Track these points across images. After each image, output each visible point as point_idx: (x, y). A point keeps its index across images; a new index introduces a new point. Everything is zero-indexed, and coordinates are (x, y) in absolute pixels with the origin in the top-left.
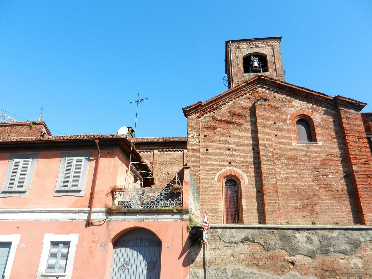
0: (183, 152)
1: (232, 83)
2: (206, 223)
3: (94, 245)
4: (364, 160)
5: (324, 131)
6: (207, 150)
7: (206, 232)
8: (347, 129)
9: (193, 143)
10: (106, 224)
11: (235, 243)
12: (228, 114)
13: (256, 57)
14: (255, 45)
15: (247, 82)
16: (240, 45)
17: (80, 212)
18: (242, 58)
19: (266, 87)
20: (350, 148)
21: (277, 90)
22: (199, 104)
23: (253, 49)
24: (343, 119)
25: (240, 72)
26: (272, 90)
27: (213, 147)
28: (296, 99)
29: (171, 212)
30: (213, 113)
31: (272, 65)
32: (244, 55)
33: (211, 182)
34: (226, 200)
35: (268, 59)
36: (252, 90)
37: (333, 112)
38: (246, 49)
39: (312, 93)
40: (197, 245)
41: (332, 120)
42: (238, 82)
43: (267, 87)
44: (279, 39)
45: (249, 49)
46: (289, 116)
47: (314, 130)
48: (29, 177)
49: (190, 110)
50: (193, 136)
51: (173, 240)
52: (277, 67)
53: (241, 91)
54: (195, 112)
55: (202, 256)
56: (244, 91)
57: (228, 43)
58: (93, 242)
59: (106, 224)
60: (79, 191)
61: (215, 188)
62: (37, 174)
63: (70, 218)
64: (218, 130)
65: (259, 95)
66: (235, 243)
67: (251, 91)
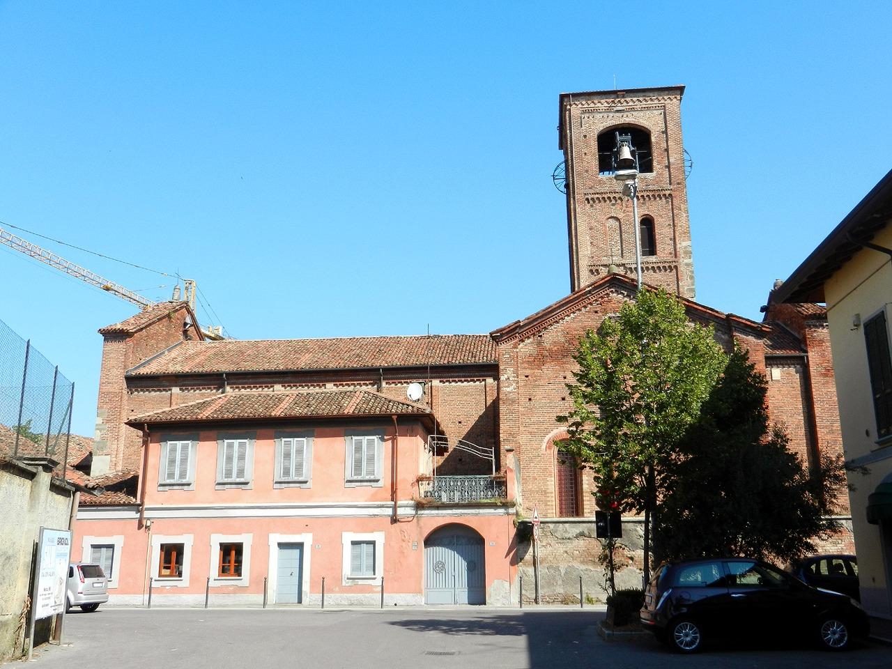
0: (483, 383)
1: (574, 198)
2: (536, 518)
3: (404, 544)
6: (530, 399)
7: (536, 527)
9: (508, 389)
11: (569, 539)
13: (626, 135)
14: (625, 104)
16: (592, 105)
17: (382, 506)
18: (596, 137)
19: (624, 292)
22: (516, 325)
25: (590, 172)
27: (539, 394)
29: (494, 506)
30: (539, 336)
31: (661, 154)
32: (601, 129)
34: (560, 476)
35: (653, 139)
36: (602, 297)
37: (725, 337)
38: (606, 115)
39: (695, 306)
40: (526, 542)
42: (587, 196)
43: (626, 293)
45: (611, 115)
48: (307, 462)
49: (502, 335)
51: (497, 537)
52: (672, 160)
54: (510, 338)
56: (589, 299)
57: (566, 100)
58: (404, 541)
60: (377, 481)
64: (547, 365)
65: (614, 305)
66: (569, 539)
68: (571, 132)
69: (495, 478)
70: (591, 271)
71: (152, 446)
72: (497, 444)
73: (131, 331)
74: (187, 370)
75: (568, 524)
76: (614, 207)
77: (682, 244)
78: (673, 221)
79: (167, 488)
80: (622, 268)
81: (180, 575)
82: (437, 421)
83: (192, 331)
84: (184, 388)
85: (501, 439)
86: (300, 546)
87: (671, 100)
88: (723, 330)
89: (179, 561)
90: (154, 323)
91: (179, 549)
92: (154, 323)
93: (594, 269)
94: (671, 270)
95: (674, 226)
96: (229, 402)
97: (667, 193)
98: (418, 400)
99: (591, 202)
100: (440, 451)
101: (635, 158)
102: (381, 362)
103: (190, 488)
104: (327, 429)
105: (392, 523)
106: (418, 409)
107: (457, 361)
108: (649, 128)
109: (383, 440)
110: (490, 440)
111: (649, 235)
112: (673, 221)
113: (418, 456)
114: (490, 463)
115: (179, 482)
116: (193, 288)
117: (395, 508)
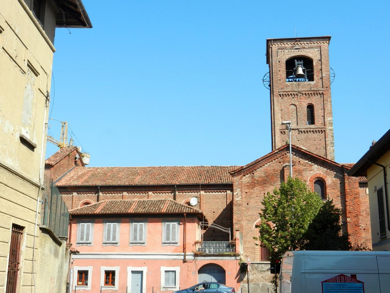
2: (249, 261)
3: (189, 273)
4: (355, 214)
5: (332, 191)
6: (248, 204)
8: (348, 190)
9: (238, 199)
10: (194, 261)
12: (264, 175)
13: (301, 61)
14: (300, 45)
15: (279, 149)
16: (283, 45)
17: (179, 255)
18: (285, 62)
19: (293, 153)
20: (347, 205)
21: (302, 156)
22: (242, 168)
23: (298, 50)
24: (346, 183)
26: (298, 156)
27: (252, 202)
28: (315, 164)
31: (318, 72)
32: (288, 58)
33: (250, 228)
35: (314, 64)
36: (283, 155)
37: (341, 176)
38: (290, 51)
39: (327, 161)
41: (339, 182)
42: (279, 93)
43: (294, 153)
44: (328, 39)
45: (293, 50)
46: (309, 178)
47: (326, 190)
49: (235, 173)
50: (238, 194)
51: (232, 270)
52: (324, 75)
53: (274, 156)
55: (247, 278)
56: (277, 156)
57: (270, 42)
58: (189, 271)
59: (194, 261)
60: (177, 243)
61: (254, 232)
62: (149, 233)
63: (174, 258)
64: (256, 188)
67: (282, 156)
68: (272, 60)
69: (230, 243)
70: (281, 132)
71: (74, 225)
72: (231, 226)
73: (53, 164)
74: (80, 184)
75: (263, 265)
76: (293, 99)
77: (328, 119)
78: (324, 107)
79: (80, 245)
80: (297, 131)
81: (87, 285)
82: (204, 216)
83: (79, 162)
84: (79, 193)
85: (234, 223)
86: (141, 272)
87: (324, 44)
88: (340, 172)
89: (86, 278)
90: (62, 159)
91: (86, 273)
92: (62, 159)
93: (283, 131)
94: (322, 132)
95: (324, 109)
96: (107, 204)
97: (321, 92)
98: (195, 205)
99: (282, 96)
100: (205, 228)
101: (305, 73)
102: (176, 182)
103: (91, 245)
104: (155, 219)
105: (183, 263)
106: (196, 210)
107: (213, 182)
108: (312, 58)
109: (179, 224)
110: (229, 221)
111: (311, 113)
112: (324, 107)
113: (195, 232)
114: (228, 234)
115: (86, 242)
116: (66, 126)
117: (185, 256)
